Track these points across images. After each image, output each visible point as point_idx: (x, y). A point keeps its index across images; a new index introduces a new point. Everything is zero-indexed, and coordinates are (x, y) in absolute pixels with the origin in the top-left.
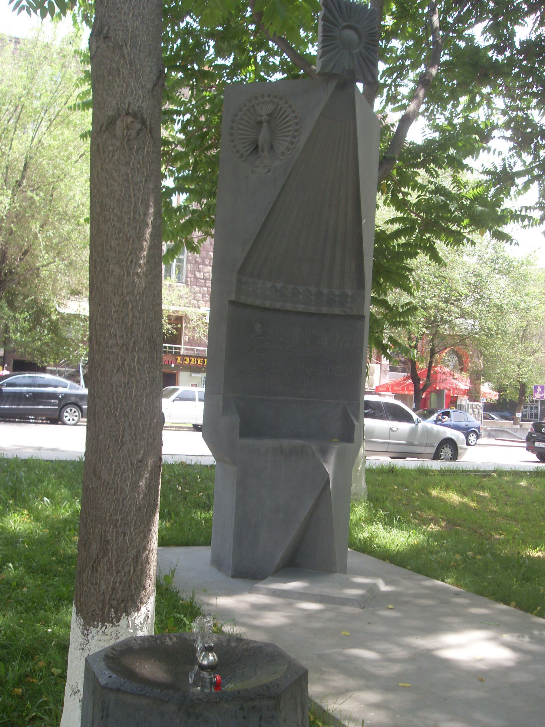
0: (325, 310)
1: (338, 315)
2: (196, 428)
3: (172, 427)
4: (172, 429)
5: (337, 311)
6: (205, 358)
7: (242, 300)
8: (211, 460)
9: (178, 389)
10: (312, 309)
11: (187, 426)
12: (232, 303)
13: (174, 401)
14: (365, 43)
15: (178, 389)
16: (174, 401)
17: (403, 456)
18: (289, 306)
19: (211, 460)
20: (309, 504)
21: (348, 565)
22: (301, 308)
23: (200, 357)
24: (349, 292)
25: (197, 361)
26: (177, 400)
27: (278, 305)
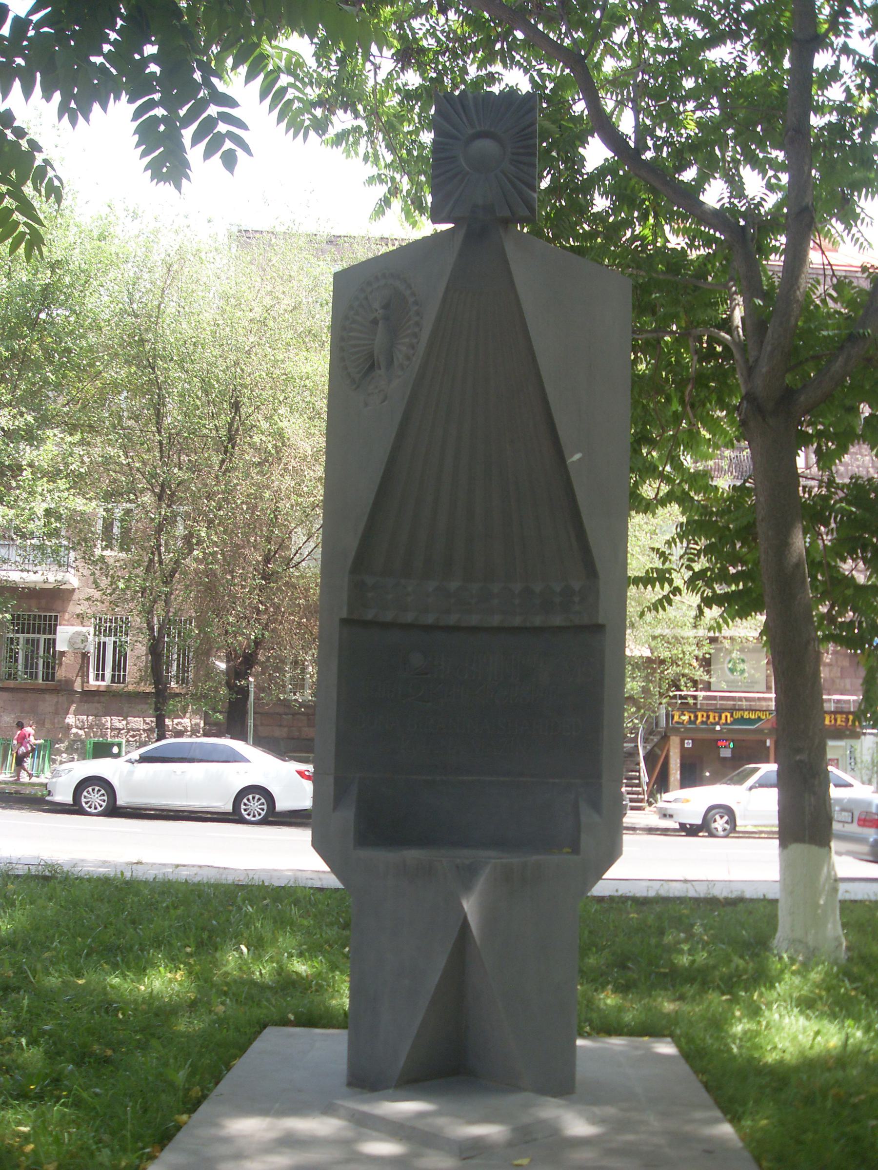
0: (538, 621)
1: (559, 628)
2: (769, 835)
3: (761, 832)
4: (763, 835)
5: (558, 620)
6: (850, 713)
7: (370, 615)
8: (333, 881)
9: (759, 768)
10: (517, 621)
11: (769, 829)
12: (343, 621)
13: (751, 789)
14: (513, 154)
15: (759, 768)
16: (751, 789)
17: (100, 867)
18: (474, 620)
19: (333, 881)
20: (440, 962)
21: (579, 1076)
22: (496, 620)
23: (841, 713)
24: (577, 585)
25: (836, 720)
26: (756, 787)
27: (452, 619)
